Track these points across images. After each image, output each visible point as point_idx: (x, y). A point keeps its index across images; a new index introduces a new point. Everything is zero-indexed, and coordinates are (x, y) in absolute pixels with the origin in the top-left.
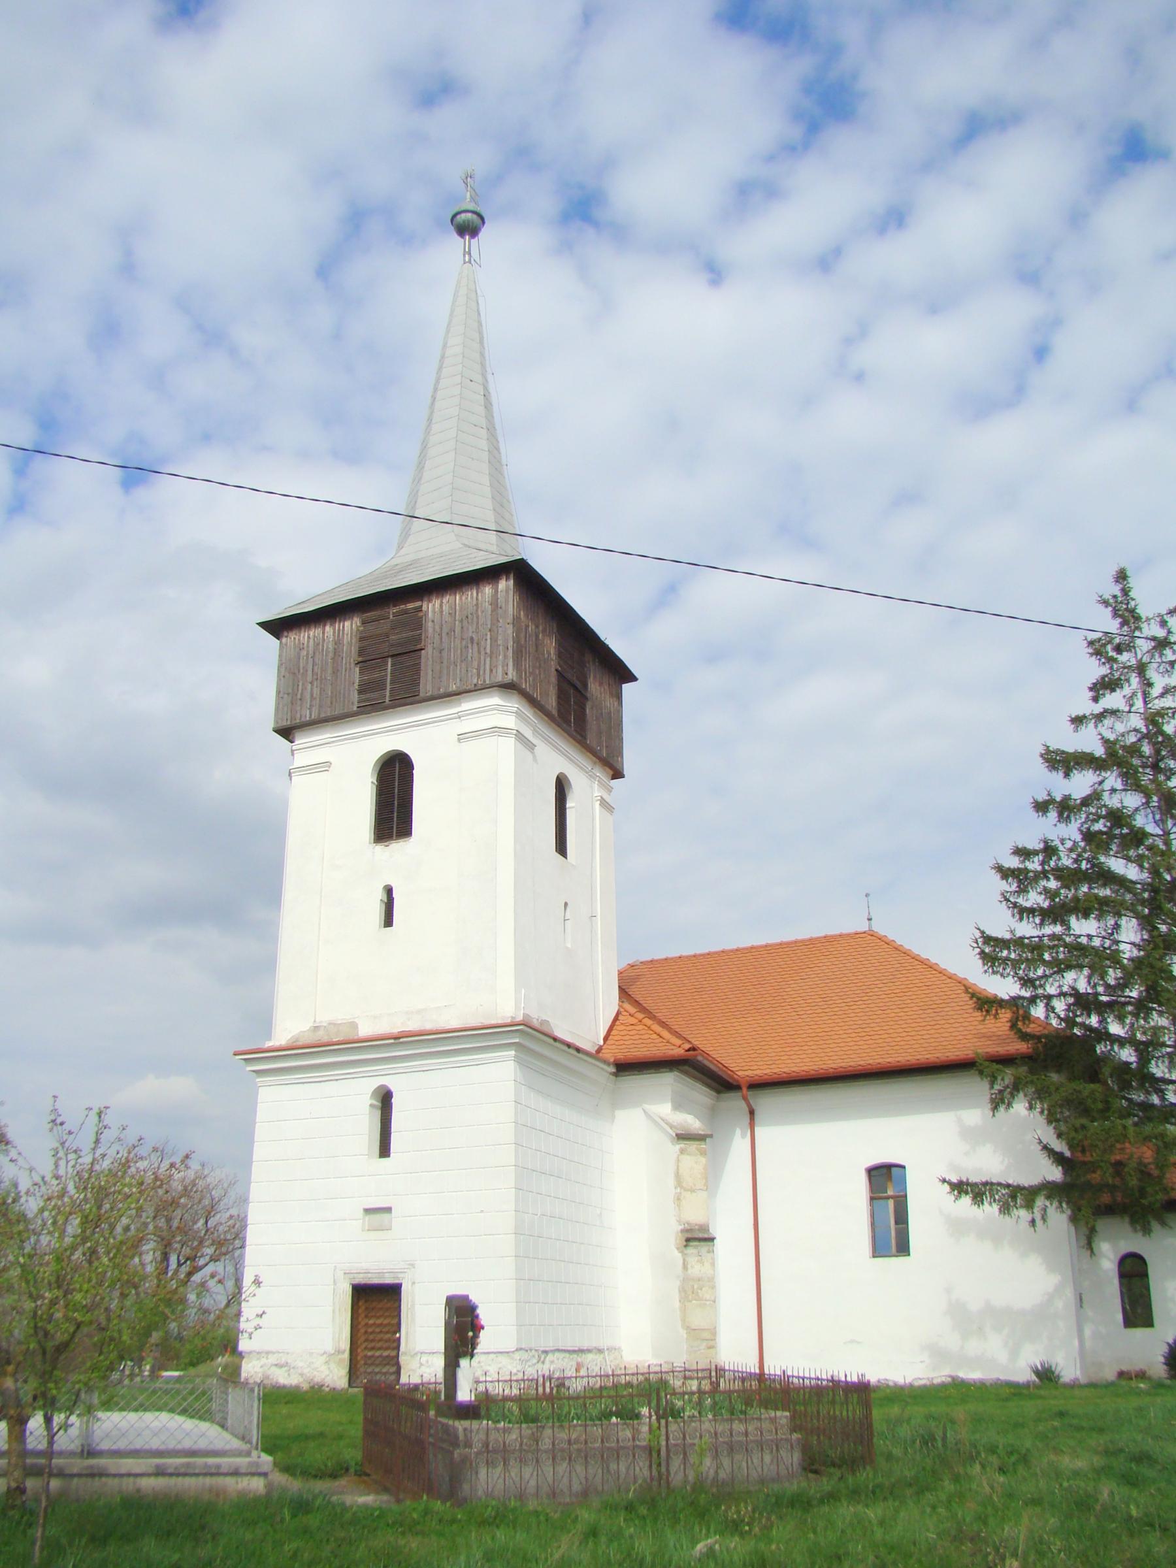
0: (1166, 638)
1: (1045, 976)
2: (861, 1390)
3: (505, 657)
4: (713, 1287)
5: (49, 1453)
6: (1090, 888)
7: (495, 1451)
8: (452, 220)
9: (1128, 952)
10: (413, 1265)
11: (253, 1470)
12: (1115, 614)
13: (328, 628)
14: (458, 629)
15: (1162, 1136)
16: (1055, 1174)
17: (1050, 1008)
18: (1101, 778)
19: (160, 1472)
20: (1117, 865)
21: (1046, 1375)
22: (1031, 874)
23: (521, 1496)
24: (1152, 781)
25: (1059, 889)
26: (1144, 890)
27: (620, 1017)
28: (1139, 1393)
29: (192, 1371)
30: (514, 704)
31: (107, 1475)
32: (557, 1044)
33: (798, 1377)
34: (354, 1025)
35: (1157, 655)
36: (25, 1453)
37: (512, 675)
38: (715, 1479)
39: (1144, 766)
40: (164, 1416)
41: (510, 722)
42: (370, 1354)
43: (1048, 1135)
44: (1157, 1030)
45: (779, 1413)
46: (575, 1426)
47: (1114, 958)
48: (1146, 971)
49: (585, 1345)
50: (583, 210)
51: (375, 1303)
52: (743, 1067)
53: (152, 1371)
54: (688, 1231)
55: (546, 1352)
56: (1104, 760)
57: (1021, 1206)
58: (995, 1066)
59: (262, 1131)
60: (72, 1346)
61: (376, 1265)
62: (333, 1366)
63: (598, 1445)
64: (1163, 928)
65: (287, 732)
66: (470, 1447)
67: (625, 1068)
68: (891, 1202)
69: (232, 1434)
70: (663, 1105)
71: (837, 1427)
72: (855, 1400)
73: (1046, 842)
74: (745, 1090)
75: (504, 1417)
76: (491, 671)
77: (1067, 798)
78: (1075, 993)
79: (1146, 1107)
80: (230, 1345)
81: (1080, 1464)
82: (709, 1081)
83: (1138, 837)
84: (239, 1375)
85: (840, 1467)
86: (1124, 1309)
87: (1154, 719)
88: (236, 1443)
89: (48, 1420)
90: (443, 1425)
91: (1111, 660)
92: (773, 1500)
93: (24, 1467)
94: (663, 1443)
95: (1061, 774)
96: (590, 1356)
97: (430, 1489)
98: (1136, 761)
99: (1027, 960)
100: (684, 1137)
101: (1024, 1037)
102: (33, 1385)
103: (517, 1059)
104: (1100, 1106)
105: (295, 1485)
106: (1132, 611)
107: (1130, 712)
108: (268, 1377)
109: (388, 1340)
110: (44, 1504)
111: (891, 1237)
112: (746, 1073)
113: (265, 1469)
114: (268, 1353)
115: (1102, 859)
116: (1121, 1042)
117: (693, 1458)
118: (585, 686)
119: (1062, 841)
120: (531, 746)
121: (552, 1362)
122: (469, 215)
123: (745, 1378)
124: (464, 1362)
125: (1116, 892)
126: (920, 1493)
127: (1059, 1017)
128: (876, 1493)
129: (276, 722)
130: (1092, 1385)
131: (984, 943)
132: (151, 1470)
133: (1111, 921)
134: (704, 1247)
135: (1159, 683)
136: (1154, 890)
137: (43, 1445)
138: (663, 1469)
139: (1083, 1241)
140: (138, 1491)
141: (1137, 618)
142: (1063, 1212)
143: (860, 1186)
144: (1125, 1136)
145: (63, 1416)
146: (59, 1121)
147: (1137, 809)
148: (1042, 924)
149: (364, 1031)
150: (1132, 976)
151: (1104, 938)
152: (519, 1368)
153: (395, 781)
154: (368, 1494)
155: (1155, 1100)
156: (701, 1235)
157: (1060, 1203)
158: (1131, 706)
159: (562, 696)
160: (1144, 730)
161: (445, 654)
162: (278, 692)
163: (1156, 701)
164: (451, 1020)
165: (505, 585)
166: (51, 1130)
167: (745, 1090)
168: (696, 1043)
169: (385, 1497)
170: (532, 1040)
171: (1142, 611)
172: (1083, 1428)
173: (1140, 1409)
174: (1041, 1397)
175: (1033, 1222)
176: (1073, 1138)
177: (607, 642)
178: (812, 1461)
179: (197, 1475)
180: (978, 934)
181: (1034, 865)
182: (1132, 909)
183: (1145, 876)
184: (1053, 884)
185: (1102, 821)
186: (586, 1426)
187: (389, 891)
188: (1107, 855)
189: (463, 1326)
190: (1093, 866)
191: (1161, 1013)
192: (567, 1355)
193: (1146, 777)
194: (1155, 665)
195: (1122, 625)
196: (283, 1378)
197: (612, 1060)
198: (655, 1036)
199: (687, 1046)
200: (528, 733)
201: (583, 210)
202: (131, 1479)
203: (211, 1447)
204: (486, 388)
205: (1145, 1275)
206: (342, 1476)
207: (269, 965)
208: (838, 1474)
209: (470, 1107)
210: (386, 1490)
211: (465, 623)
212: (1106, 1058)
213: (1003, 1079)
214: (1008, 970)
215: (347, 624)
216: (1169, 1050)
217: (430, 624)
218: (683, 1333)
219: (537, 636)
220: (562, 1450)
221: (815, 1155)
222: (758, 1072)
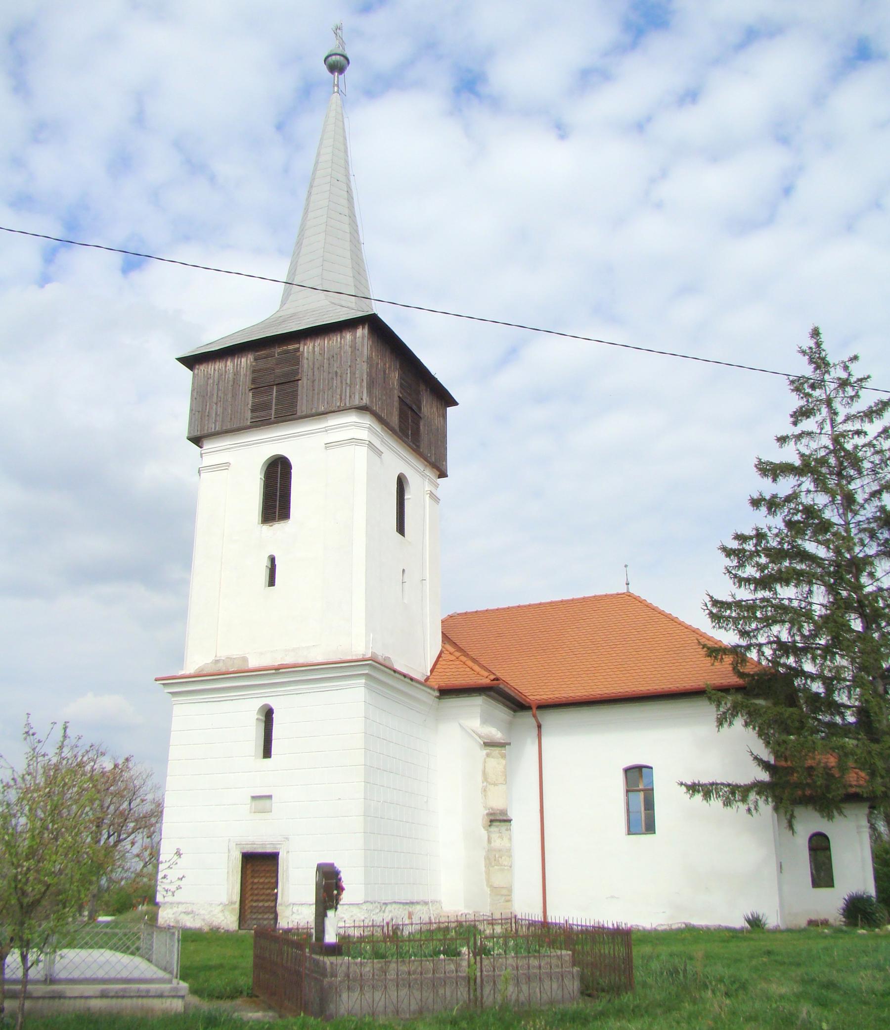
0: (847, 379)
1: (757, 629)
2: (622, 936)
3: (361, 386)
4: (510, 856)
5: (25, 981)
6: (790, 563)
7: (355, 980)
8: (325, 61)
9: (818, 611)
10: (287, 839)
11: (173, 994)
12: (811, 361)
13: (229, 363)
14: (326, 365)
15: (843, 747)
16: (764, 776)
17: (761, 653)
18: (799, 482)
19: (104, 995)
20: (811, 547)
21: (755, 923)
22: (748, 553)
23: (373, 1014)
24: (837, 485)
25: (768, 564)
26: (830, 565)
27: (443, 655)
28: (826, 937)
29: (121, 918)
30: (367, 421)
31: (65, 998)
32: (397, 675)
33: (577, 925)
34: (245, 659)
35: (841, 393)
37: (366, 400)
38: (517, 1000)
39: (831, 474)
41: (364, 434)
42: (255, 904)
44: (839, 669)
45: (564, 952)
46: (414, 961)
47: (808, 615)
48: (831, 625)
49: (415, 899)
50: (470, 86)
51: (259, 866)
52: (534, 693)
54: (491, 814)
55: (386, 904)
56: (802, 470)
57: (739, 801)
58: (720, 694)
59: (174, 738)
61: (260, 838)
62: (227, 913)
63: (430, 975)
64: (844, 593)
65: (197, 440)
66: (336, 976)
67: (446, 692)
68: (642, 794)
69: (156, 965)
70: (474, 719)
71: (606, 960)
72: (620, 940)
73: (757, 530)
74: (534, 709)
75: (361, 954)
76: (350, 397)
77: (774, 496)
78: (778, 642)
79: (831, 725)
80: (149, 896)
81: (783, 990)
82: (508, 703)
83: (825, 526)
84: (157, 920)
85: (608, 992)
86: (812, 873)
87: (837, 439)
88: (161, 974)
89: (24, 958)
90: (314, 960)
91: (808, 395)
92: (560, 1017)
94: (479, 974)
95: (770, 479)
96: (418, 907)
97: (305, 1007)
98: (824, 470)
99: (744, 617)
100: (489, 744)
101: (741, 675)
103: (366, 686)
104: (797, 724)
105: (206, 1006)
106: (823, 359)
107: (820, 433)
108: (178, 922)
109: (268, 895)
110: (20, 1020)
111: (643, 819)
113: (181, 993)
115: (800, 542)
116: (812, 677)
117: (501, 986)
118: (420, 408)
119: (770, 529)
120: (379, 453)
121: (391, 911)
122: (338, 58)
123: (532, 924)
124: (330, 913)
125: (809, 566)
126: (669, 1010)
127: (767, 659)
129: (189, 432)
130: (789, 931)
132: (98, 994)
133: (806, 588)
134: (503, 826)
135: (842, 412)
136: (838, 565)
138: (478, 994)
139: (785, 823)
140: (89, 1009)
141: (827, 364)
144: (814, 749)
147: (825, 506)
148: (755, 590)
149: (253, 663)
150: (821, 629)
151: (800, 600)
152: (366, 915)
153: (278, 474)
154: (258, 1011)
155: (838, 720)
156: (501, 818)
157: (767, 797)
158: (822, 429)
159: (402, 416)
160: (831, 447)
161: (316, 383)
162: (191, 410)
163: (840, 426)
164: (317, 656)
165: (362, 332)
166: (25, 739)
167: (534, 709)
168: (499, 675)
169: (271, 1014)
170: (378, 670)
171: (830, 359)
172: (784, 963)
173: (826, 949)
174: (752, 939)
176: (778, 751)
178: (587, 987)
179: (131, 997)
180: (707, 599)
181: (750, 546)
182: (821, 578)
183: (831, 554)
184: (763, 560)
185: (800, 514)
186: (421, 961)
187: (272, 560)
188: (803, 539)
189: (329, 887)
190: (793, 547)
191: (842, 656)
192: (401, 906)
193: (832, 482)
194: (839, 399)
195: (816, 369)
196: (190, 923)
197: (436, 687)
198: (468, 669)
199: (492, 677)
200: (377, 443)
201: (470, 86)
202: (83, 1001)
203: (143, 976)
204: (349, 186)
205: (828, 848)
206: (237, 997)
207: (182, 614)
208: (608, 997)
209: (329, 723)
210: (270, 1008)
212: (807, 690)
213: (726, 704)
214: (730, 625)
215: (244, 360)
216: (848, 683)
217: (305, 361)
218: (488, 890)
220: (403, 980)
221: (586, 758)
222: (545, 697)
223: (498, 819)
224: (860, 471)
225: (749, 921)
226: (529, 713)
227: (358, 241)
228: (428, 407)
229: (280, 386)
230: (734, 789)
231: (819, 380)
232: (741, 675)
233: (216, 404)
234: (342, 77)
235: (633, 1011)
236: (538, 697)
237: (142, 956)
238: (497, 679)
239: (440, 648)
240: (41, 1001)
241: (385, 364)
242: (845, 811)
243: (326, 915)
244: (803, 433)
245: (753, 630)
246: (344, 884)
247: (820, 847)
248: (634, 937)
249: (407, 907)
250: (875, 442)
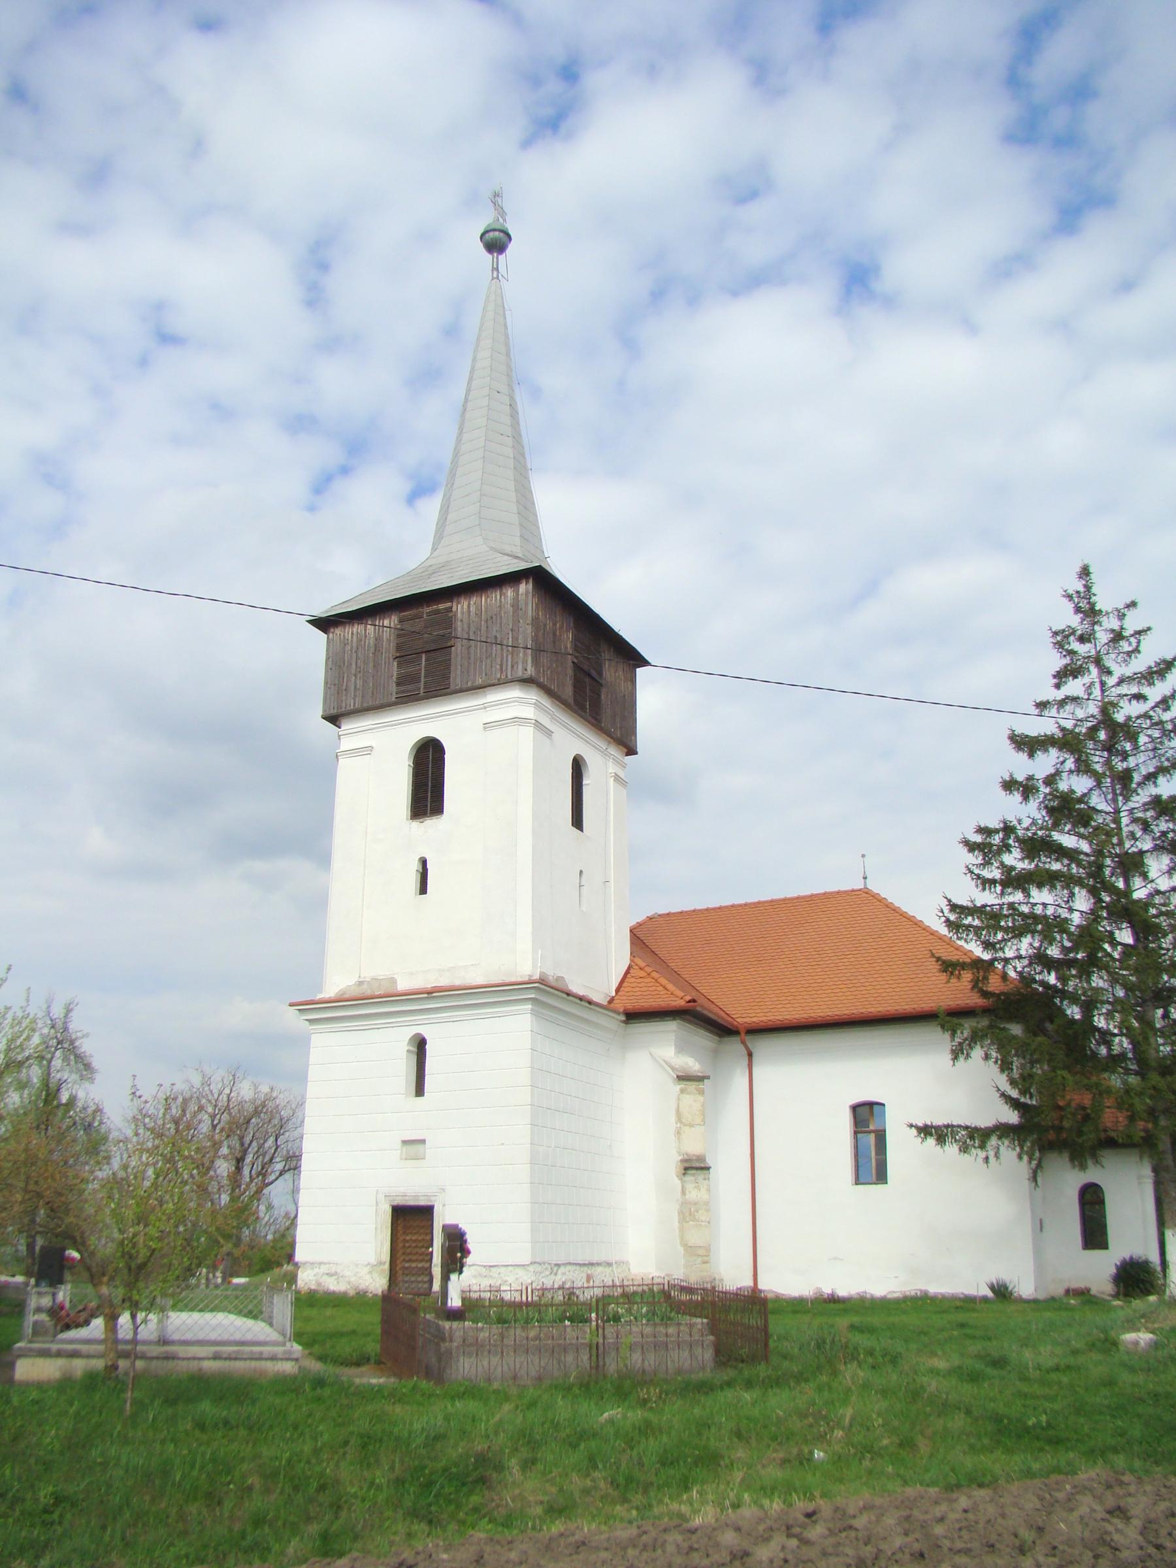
1: (1004, 940)
5: (134, 1341)
7: (471, 1345)
12: (1078, 610)
14: (483, 628)
16: (1012, 1117)
19: (216, 1357)
21: (1001, 1292)
30: (533, 695)
31: (179, 1358)
34: (393, 981)
36: (116, 1341)
37: (530, 671)
40: (232, 1317)
41: (529, 712)
42: (407, 1265)
43: (1003, 1082)
49: (595, 1260)
53: (224, 1279)
55: (558, 1265)
60: (149, 1265)
61: (413, 1191)
62: (375, 1275)
65: (334, 719)
67: (633, 1016)
68: (872, 1136)
70: (667, 1048)
73: (1005, 823)
74: (743, 1034)
77: (1030, 778)
84: (296, 1282)
89: (133, 1317)
91: (1071, 653)
93: (117, 1351)
96: (599, 1269)
100: (684, 1078)
101: (985, 994)
102: (121, 1292)
105: (316, 1366)
108: (319, 1284)
111: (871, 1165)
113: (295, 1356)
114: (320, 1263)
118: (600, 674)
120: (549, 733)
121: (564, 1274)
122: (497, 234)
126: (798, 1382)
128: (777, 1382)
129: (324, 710)
131: (951, 911)
132: (211, 1355)
134: (700, 1175)
137: (130, 1336)
140: (200, 1370)
142: (1014, 1149)
143: (844, 1123)
145: (144, 1314)
146: (138, 1094)
148: (1002, 894)
149: (403, 985)
152: (533, 1278)
153: (429, 761)
156: (698, 1165)
158: (1089, 694)
159: (578, 686)
165: (525, 588)
167: (743, 1034)
169: (392, 1380)
170: (549, 995)
175: (987, 1158)
177: (621, 633)
179: (245, 1359)
187: (424, 862)
196: (333, 1285)
198: (661, 988)
199: (688, 998)
200: (546, 721)
202: (196, 1362)
203: (255, 1339)
205: (1102, 1202)
209: (491, 1051)
210: (395, 1375)
211: (490, 622)
217: (459, 623)
218: (681, 1250)
219: (554, 634)
221: (805, 1094)
223: (694, 1167)
224: (1136, 747)
225: (992, 1288)
226: (738, 1039)
227: (525, 467)
228: (611, 671)
229: (432, 654)
231: (1088, 636)
232: (985, 994)
233: (355, 676)
234: (502, 257)
235: (763, 1381)
236: (747, 1020)
237: (263, 1320)
238: (694, 1001)
239: (628, 962)
240: (155, 1362)
241: (555, 624)
242: (1104, 1161)
243: (448, 1279)
244: (1067, 698)
245: (999, 942)
246: (471, 1245)
247: (1092, 1203)
248: (770, 1305)
249: (585, 1269)
250: (1151, 713)
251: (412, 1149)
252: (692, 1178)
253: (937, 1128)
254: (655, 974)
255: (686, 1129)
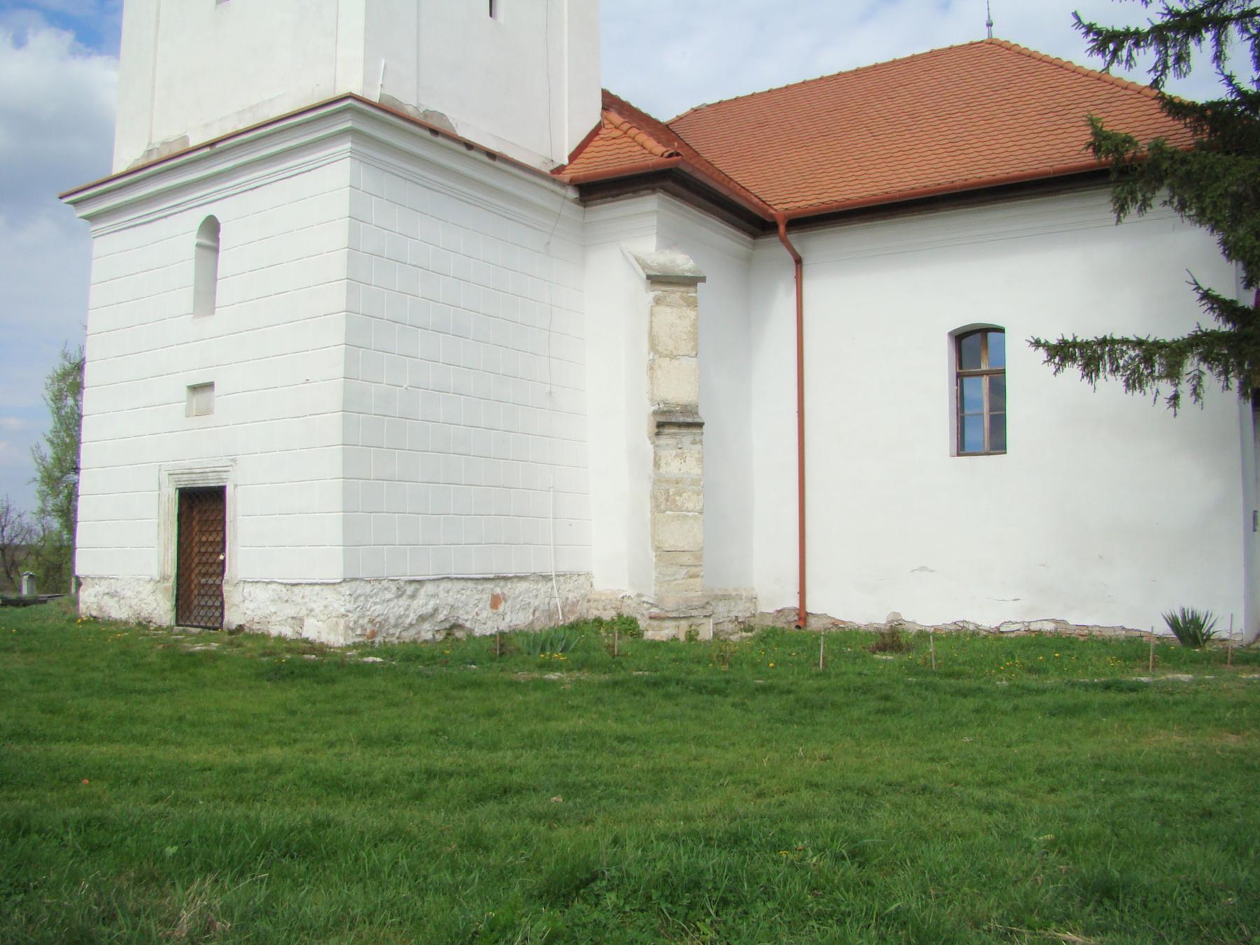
16: (1212, 323)
21: (1189, 631)
32: (440, 139)
34: (185, 139)
42: (203, 581)
49: (511, 571)
52: (780, 193)
54: (663, 413)
61: (199, 460)
62: (160, 596)
68: (985, 381)
70: (645, 234)
100: (659, 280)
108: (100, 609)
111: (981, 424)
112: (785, 206)
114: (101, 578)
121: (435, 596)
134: (687, 436)
143: (942, 357)
156: (681, 419)
167: (782, 228)
170: (394, 132)
175: (1175, 398)
192: (470, 585)
218: (652, 554)
221: (882, 315)
230: (1149, 350)
249: (489, 586)
251: (201, 397)
252: (672, 441)
253: (1085, 345)
254: (633, 132)
255: (665, 362)
